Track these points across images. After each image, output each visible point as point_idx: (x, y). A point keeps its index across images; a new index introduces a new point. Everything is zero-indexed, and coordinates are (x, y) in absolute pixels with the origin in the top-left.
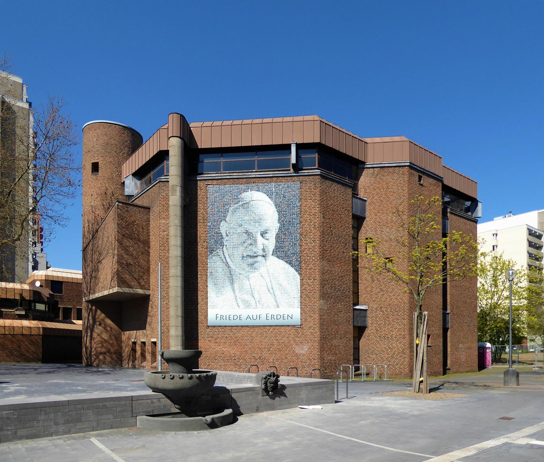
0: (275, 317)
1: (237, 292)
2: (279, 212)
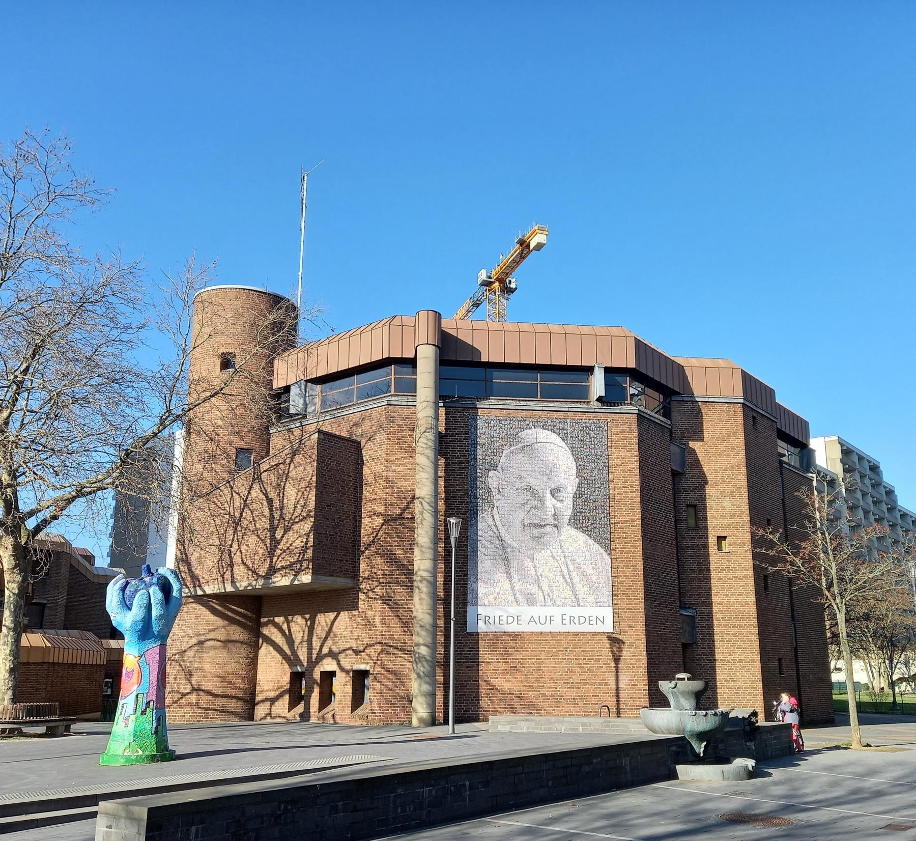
0: (576, 621)
2: (576, 460)
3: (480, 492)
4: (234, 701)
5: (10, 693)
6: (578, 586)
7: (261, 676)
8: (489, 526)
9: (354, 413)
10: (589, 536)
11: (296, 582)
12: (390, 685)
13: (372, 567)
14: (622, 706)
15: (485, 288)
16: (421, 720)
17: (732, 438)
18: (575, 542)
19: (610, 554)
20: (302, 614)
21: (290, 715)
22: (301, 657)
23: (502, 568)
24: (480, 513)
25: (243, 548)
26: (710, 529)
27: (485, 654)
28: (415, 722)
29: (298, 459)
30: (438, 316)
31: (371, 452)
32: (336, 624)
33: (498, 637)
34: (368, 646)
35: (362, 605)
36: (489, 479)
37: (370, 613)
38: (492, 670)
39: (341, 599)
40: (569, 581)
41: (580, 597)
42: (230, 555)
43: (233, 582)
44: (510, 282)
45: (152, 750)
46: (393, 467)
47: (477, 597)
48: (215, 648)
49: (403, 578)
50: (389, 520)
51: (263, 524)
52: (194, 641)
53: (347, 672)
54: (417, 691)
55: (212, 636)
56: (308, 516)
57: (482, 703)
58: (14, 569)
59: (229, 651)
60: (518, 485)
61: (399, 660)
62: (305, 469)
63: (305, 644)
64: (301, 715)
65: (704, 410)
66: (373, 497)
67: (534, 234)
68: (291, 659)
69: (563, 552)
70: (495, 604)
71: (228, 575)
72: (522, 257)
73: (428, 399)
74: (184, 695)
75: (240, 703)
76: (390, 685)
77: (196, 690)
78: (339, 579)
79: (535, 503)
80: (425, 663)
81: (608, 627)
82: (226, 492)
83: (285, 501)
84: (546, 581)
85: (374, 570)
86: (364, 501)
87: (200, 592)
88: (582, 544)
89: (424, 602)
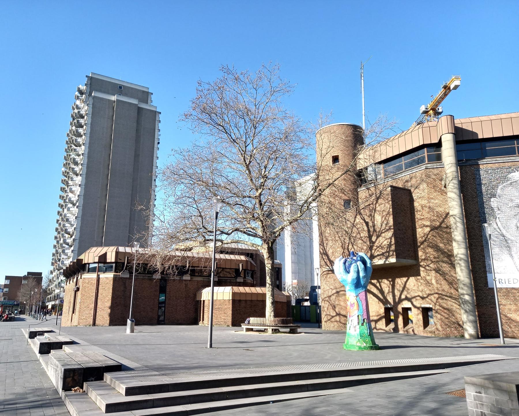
3: (486, 210)
5: (273, 313)
8: (495, 229)
9: (405, 175)
11: (387, 262)
12: (446, 316)
13: (426, 253)
16: (471, 335)
21: (387, 329)
22: (390, 300)
23: (506, 252)
27: (499, 299)
28: (467, 336)
29: (380, 201)
30: (452, 117)
31: (418, 194)
32: (408, 283)
33: (508, 292)
34: (429, 295)
35: (422, 274)
36: (492, 203)
37: (428, 278)
39: (410, 269)
42: (348, 250)
44: (438, 109)
45: (370, 344)
46: (432, 201)
49: (446, 259)
50: (433, 228)
51: (365, 234)
52: (334, 291)
53: (418, 308)
56: (390, 229)
60: (510, 204)
61: (449, 303)
62: (385, 206)
63: (391, 294)
64: (394, 329)
66: (422, 217)
67: (452, 81)
68: (384, 301)
72: (445, 95)
74: (333, 317)
76: (446, 316)
78: (409, 260)
80: (469, 305)
83: (376, 222)
85: (428, 255)
86: (416, 220)
89: (464, 271)
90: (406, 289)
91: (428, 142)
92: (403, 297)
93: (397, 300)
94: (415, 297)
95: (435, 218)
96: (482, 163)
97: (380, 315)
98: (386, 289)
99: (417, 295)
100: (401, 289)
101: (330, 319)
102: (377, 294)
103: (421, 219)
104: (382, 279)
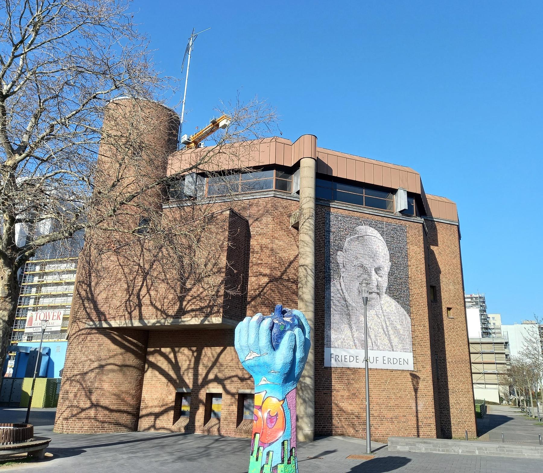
0: (392, 361)
1: (354, 330)
2: (389, 249)
3: (332, 265)
4: (125, 415)
6: (392, 337)
7: (145, 395)
8: (338, 290)
10: (398, 302)
11: (206, 322)
14: (420, 424)
15: (185, 145)
16: (306, 436)
17: (453, 246)
18: (388, 305)
19: (410, 316)
20: (189, 347)
21: (174, 428)
22: (187, 381)
23: (346, 321)
24: (332, 280)
25: (152, 293)
26: (443, 302)
27: (336, 384)
31: (257, 229)
32: (222, 356)
36: (338, 257)
38: (341, 398)
40: (387, 332)
41: (393, 344)
43: (141, 319)
44: (200, 144)
46: (276, 241)
47: (330, 341)
48: (113, 371)
50: (273, 279)
51: (173, 274)
52: (96, 364)
53: (233, 395)
54: (303, 413)
55: (111, 361)
56: (219, 271)
57: (334, 422)
58: (6, 297)
59: (124, 374)
60: (355, 263)
63: (191, 371)
64: (186, 428)
65: (438, 227)
66: (259, 262)
68: (177, 382)
69: (383, 312)
70: (342, 347)
71: (136, 313)
72: (212, 131)
73: (311, 196)
74: (83, 410)
75: (129, 417)
77: (95, 406)
79: (366, 276)
80: (309, 391)
81: (410, 367)
82: (138, 248)
84: (373, 332)
86: (250, 265)
87: (105, 325)
88: (394, 308)
90: (218, 364)
91: (280, 163)
92: (211, 376)
93: (200, 380)
94: (230, 378)
95: (277, 265)
96: (333, 206)
97: (167, 404)
98: (184, 363)
99: (233, 374)
100: (210, 365)
101: (78, 414)
102: (166, 370)
103: (258, 264)
104: (180, 346)
